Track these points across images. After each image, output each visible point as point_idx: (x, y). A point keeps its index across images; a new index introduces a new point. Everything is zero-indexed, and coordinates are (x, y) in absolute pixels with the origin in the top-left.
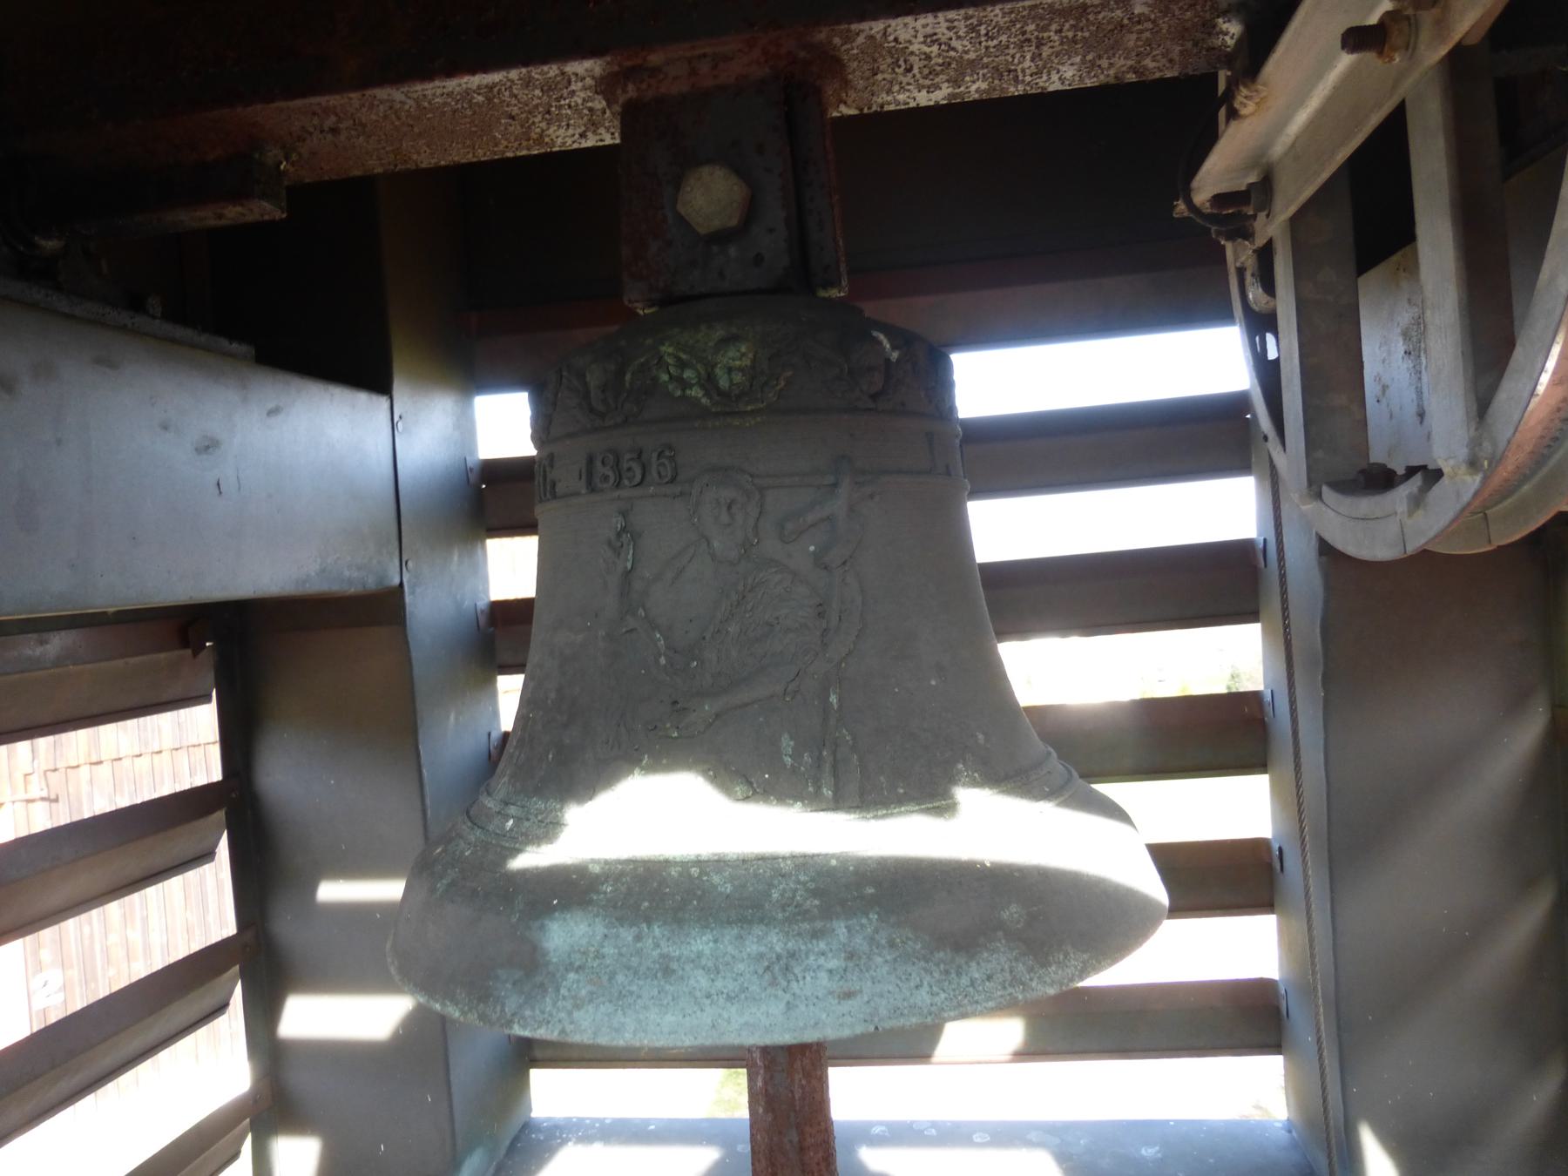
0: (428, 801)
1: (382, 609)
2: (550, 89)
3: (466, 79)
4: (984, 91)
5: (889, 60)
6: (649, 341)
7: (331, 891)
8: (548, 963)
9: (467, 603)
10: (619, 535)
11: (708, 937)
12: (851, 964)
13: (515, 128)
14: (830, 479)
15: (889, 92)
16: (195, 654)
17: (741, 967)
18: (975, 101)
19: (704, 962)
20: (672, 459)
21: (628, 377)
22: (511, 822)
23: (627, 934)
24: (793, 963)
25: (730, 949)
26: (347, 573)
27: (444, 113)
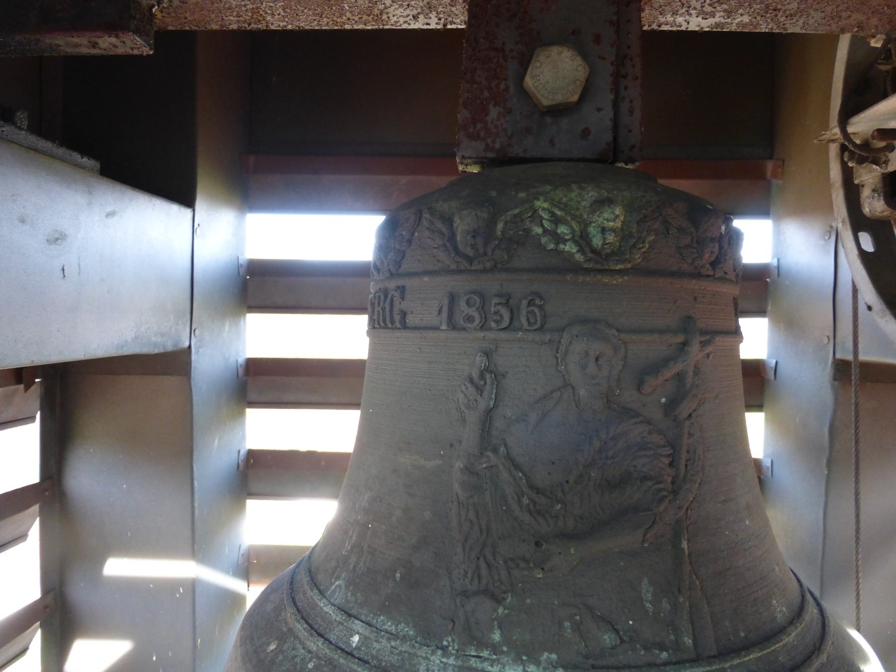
0: (196, 505)
1: (174, 364)
4: (746, 24)
6: (522, 195)
7: (117, 567)
9: (232, 360)
10: (482, 376)
14: (680, 338)
16: (27, 388)
18: (731, 33)
20: (541, 307)
21: (500, 226)
26: (153, 339)
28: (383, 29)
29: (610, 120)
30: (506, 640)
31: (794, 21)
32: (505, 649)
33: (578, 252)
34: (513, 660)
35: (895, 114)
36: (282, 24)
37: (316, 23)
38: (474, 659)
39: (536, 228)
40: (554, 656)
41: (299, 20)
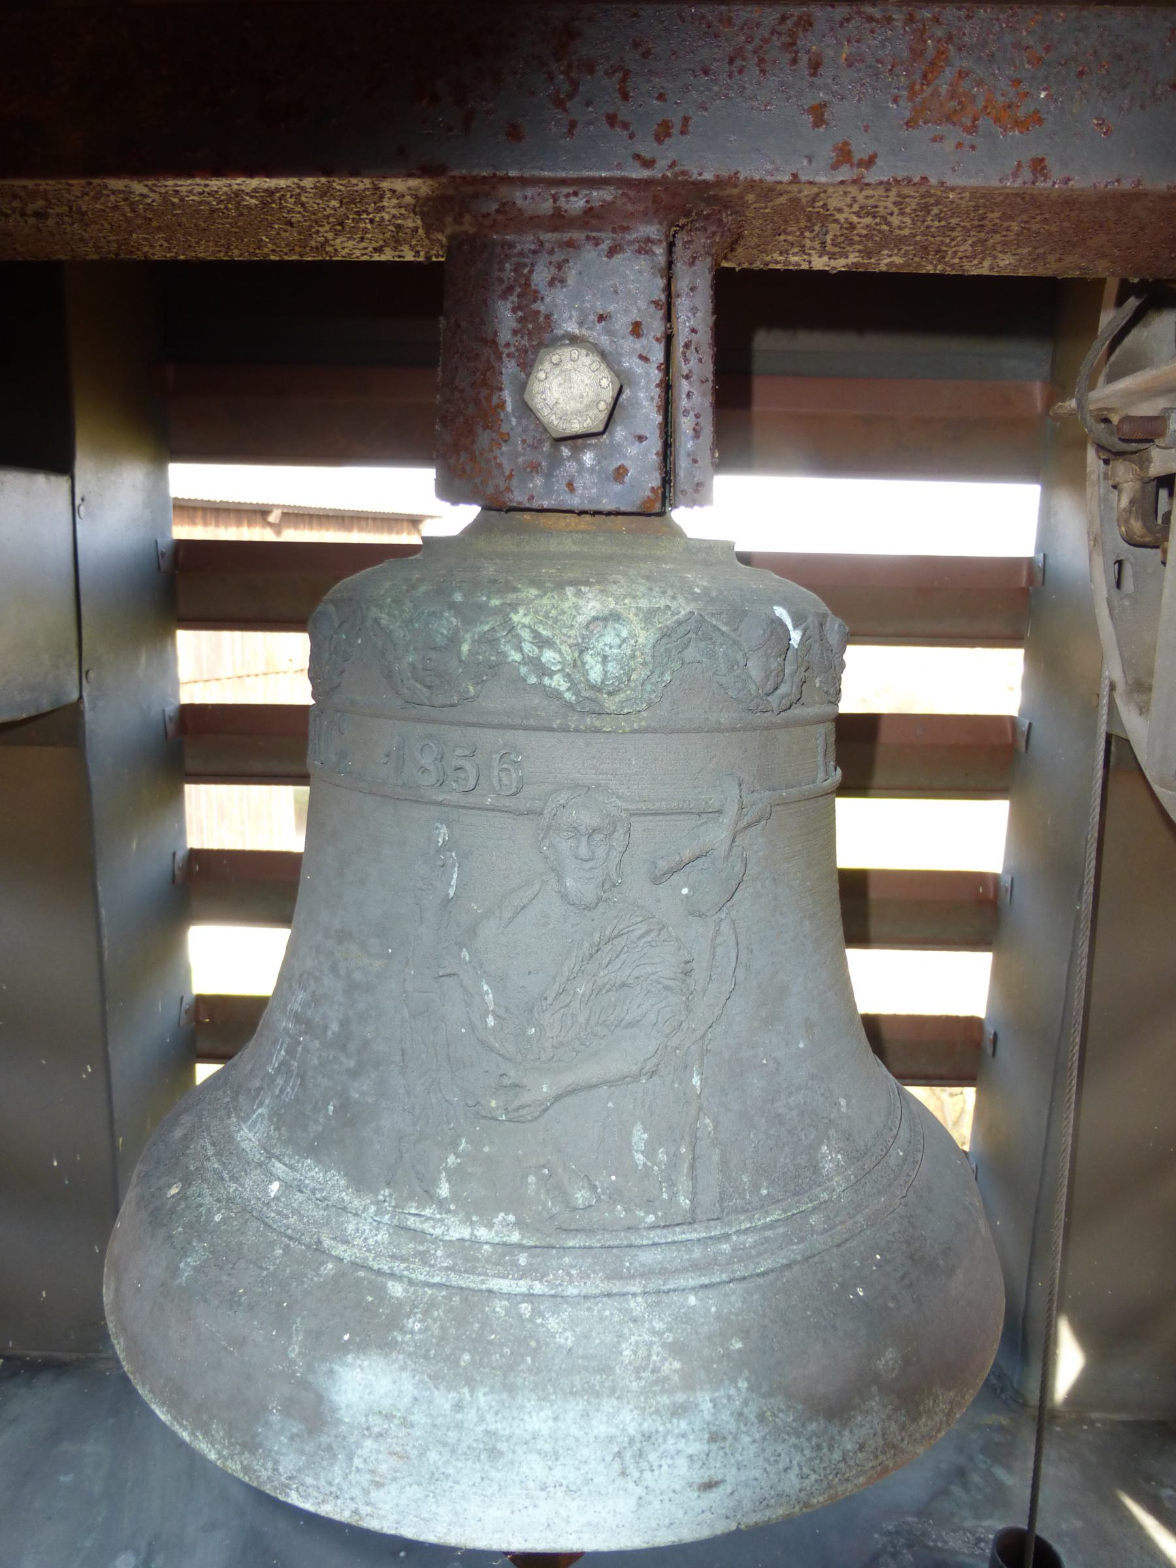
0: (105, 943)
1: (59, 727)
2: (353, 201)
3: (239, 181)
5: (803, 224)
6: (495, 602)
8: (338, 1422)
11: (547, 1413)
12: (714, 1447)
17: (585, 1452)
18: (881, 273)
19: (540, 1444)
22: (275, 1187)
23: (444, 1400)
24: (648, 1447)
25: (574, 1430)
27: (198, 211)
28: (331, 262)
29: (657, 454)
30: (455, 1196)
31: (975, 262)
32: (452, 1207)
33: (568, 689)
34: (461, 1222)
36: (168, 255)
39: (513, 652)
40: (511, 1218)
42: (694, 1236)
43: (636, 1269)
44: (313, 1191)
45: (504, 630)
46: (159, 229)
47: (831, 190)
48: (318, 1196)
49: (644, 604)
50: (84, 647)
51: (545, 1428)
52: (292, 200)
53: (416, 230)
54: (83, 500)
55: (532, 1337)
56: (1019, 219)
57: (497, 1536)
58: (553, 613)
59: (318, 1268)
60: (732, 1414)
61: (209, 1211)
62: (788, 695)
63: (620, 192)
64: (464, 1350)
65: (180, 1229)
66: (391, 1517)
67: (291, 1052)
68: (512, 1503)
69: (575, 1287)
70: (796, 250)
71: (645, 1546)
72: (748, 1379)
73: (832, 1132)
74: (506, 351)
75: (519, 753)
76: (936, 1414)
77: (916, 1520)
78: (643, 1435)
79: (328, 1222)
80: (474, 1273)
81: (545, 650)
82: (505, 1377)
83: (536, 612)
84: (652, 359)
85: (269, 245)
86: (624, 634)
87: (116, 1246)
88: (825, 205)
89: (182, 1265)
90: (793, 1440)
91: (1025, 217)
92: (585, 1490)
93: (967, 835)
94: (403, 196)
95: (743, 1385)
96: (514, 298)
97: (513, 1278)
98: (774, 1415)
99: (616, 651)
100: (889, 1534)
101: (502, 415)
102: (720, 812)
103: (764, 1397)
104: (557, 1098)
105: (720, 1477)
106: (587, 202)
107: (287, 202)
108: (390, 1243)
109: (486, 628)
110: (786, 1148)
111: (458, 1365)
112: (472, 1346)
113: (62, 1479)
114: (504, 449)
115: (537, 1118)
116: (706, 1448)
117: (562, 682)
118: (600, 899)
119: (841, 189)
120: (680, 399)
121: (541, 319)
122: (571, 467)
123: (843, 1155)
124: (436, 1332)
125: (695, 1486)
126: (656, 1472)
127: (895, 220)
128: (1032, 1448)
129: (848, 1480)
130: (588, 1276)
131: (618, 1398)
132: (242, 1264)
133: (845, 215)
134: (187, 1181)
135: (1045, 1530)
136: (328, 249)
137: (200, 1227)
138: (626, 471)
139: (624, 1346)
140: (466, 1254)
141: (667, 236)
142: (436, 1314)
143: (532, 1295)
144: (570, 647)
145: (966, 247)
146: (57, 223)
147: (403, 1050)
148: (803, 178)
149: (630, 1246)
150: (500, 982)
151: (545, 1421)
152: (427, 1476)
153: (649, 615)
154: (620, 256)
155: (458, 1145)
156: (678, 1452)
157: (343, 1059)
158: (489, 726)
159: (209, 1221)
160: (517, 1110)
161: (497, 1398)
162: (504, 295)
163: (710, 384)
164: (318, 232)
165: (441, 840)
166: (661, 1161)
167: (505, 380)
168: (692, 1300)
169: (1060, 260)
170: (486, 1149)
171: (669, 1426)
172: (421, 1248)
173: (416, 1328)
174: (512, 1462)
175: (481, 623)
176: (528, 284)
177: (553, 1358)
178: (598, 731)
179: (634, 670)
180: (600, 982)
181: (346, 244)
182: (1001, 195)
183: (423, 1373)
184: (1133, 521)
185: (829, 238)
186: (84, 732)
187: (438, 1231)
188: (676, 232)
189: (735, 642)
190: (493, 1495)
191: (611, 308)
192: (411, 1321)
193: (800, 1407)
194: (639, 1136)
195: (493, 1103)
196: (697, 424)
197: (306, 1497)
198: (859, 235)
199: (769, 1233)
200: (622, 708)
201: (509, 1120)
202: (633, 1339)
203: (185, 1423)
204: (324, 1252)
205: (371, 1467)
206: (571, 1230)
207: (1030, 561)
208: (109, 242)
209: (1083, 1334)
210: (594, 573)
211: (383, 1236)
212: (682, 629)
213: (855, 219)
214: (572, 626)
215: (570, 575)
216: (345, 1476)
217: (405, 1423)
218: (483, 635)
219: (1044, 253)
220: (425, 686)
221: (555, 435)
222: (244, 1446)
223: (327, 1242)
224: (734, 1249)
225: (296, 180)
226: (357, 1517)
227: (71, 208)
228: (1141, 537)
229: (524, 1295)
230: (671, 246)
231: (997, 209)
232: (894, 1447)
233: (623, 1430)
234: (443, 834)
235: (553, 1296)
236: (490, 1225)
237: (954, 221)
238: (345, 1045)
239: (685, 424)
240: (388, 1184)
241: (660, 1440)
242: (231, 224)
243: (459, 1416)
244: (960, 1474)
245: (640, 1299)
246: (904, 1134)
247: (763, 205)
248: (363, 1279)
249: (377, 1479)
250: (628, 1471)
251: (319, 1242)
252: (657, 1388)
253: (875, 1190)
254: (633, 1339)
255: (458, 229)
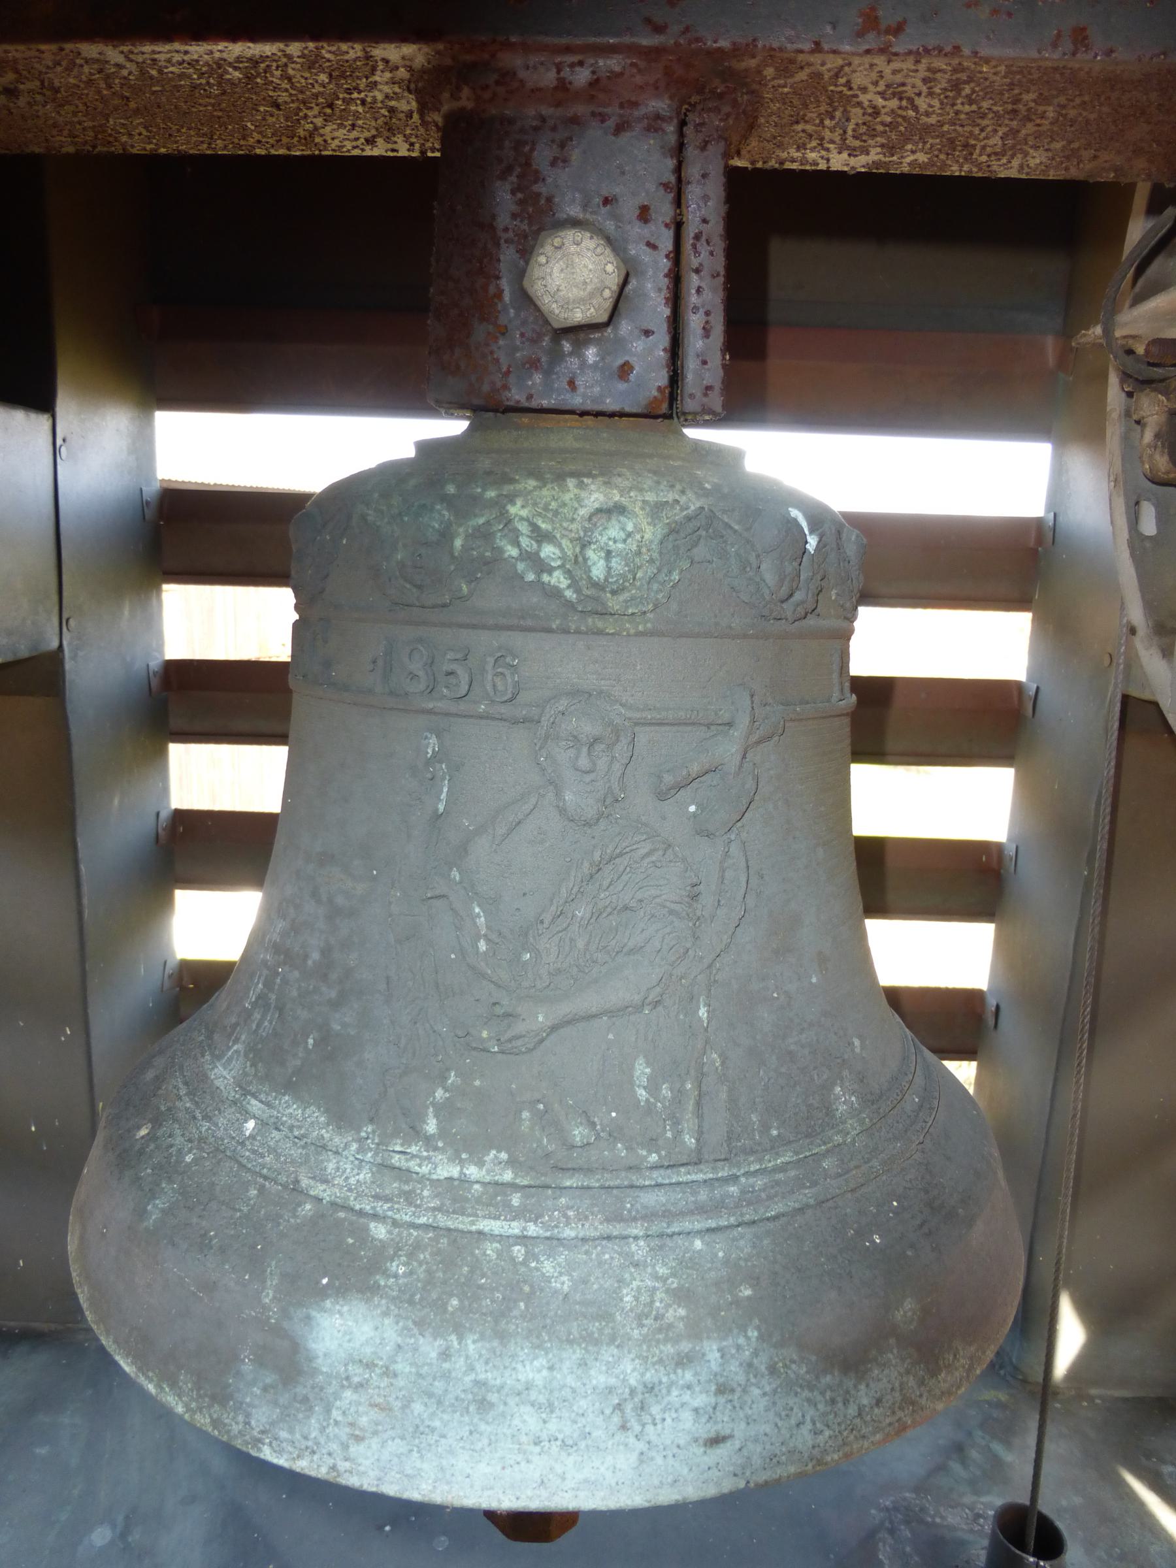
0: (85, 901)
2: (343, 76)
3: (221, 46)
5: (823, 109)
6: (491, 494)
8: (315, 1372)
9: (139, 665)
11: (541, 1362)
12: (722, 1400)
13: (278, 120)
15: (801, 147)
18: (902, 175)
19: (533, 1395)
22: (251, 1124)
23: (430, 1348)
24: (650, 1399)
25: (570, 1381)
27: (178, 88)
28: (320, 156)
29: (665, 350)
30: (443, 1132)
31: (1004, 161)
32: (440, 1144)
33: (569, 587)
34: (449, 1159)
35: (1175, 316)
36: (149, 147)
37: (205, 146)
38: (398, 1156)
39: (509, 547)
40: (504, 1156)
41: (176, 142)
42: (700, 1177)
43: (637, 1211)
44: (291, 1128)
45: (499, 523)
46: (137, 111)
47: (856, 61)
48: (296, 1133)
49: (651, 497)
50: (65, 594)
51: (539, 1379)
52: (278, 73)
53: (409, 115)
54: (64, 440)
55: (525, 1282)
56: (1056, 101)
57: (487, 1493)
58: (554, 505)
59: (295, 1210)
60: (741, 1364)
61: (180, 1151)
62: (803, 602)
63: (629, 61)
64: (451, 1295)
65: (149, 1171)
66: (371, 1474)
67: (268, 985)
68: (503, 1458)
69: (572, 1229)
70: (814, 143)
71: (647, 1505)
72: (758, 1328)
73: (846, 1073)
74: (504, 236)
75: (514, 657)
76: (956, 1369)
77: (914, 1496)
78: (645, 1386)
79: (307, 1161)
80: (463, 1214)
81: (544, 545)
82: (496, 1322)
83: (535, 504)
84: (661, 246)
85: (255, 134)
86: (630, 527)
87: (82, 1192)
88: (849, 82)
89: (149, 1207)
90: (806, 1393)
91: (1062, 100)
92: (582, 1444)
93: (966, 803)
94: (397, 68)
95: (753, 1334)
96: (513, 179)
97: (505, 1220)
98: (785, 1366)
99: (620, 546)
100: (887, 1509)
101: (500, 307)
102: (730, 724)
103: (775, 1346)
104: (554, 1028)
105: (727, 1432)
106: (593, 72)
107: (273, 76)
108: (373, 1182)
109: (481, 521)
110: (798, 1088)
111: (445, 1311)
112: (459, 1291)
113: (38, 1451)
114: (501, 342)
115: (530, 1051)
116: (713, 1400)
117: (562, 579)
118: (601, 815)
119: (867, 59)
120: (689, 294)
121: (543, 202)
122: (573, 363)
123: (857, 1098)
124: (422, 1276)
125: (701, 1442)
126: (659, 1426)
127: (922, 103)
128: (1033, 1425)
129: (864, 1437)
130: (586, 1218)
131: (618, 1347)
132: (214, 1205)
133: (869, 96)
134: (157, 1122)
135: (1046, 1506)
136: (318, 140)
137: (170, 1169)
138: (632, 368)
139: (625, 1291)
140: (454, 1193)
141: (678, 113)
142: (422, 1256)
143: (525, 1237)
144: (571, 541)
145: (996, 140)
146: (29, 103)
147: (388, 978)
148: (826, 47)
149: (632, 1186)
150: (492, 904)
151: (539, 1371)
152: (411, 1430)
153: (656, 510)
154: (628, 134)
155: (446, 1078)
156: (683, 1405)
157: (324, 989)
158: (484, 627)
159: (179, 1162)
160: (510, 1041)
161: (488, 1345)
162: (503, 176)
163: (721, 279)
164: (306, 116)
165: (430, 751)
166: (665, 1098)
167: (503, 267)
168: (698, 1244)
169: (1095, 157)
170: (477, 1083)
171: (673, 1376)
172: (406, 1188)
173: (400, 1272)
174: (503, 1415)
175: (475, 516)
176: (528, 164)
177: (548, 1304)
178: (600, 633)
179: (639, 568)
180: (601, 905)
181: (336, 134)
182: (1039, 68)
183: (407, 1318)
184: (1157, 457)
185: (851, 126)
186: (64, 682)
187: (425, 1169)
188: (687, 110)
189: (748, 542)
190: (482, 1449)
191: (617, 190)
192: (394, 1264)
193: (814, 1358)
194: (642, 1070)
195: (485, 1034)
196: (707, 322)
197: (280, 1452)
198: (883, 124)
199: (780, 1176)
200: (627, 608)
201: (502, 1052)
202: (635, 1284)
203: (150, 1374)
204: (302, 1192)
205: (350, 1419)
206: (568, 1169)
207: (1039, 522)
208: (84, 129)
209: (1084, 1309)
210: (601, 468)
211: (365, 1175)
212: (692, 525)
213: (880, 102)
214: (573, 520)
215: (572, 467)
216: (323, 1429)
217: (388, 1372)
218: (477, 529)
219: (1079, 148)
220: (415, 586)
221: (556, 325)
222: (214, 1398)
223: (305, 1182)
224: (743, 1192)
225: (281, 45)
226: (335, 1474)
227: (42, 82)
228: (1168, 473)
229: (518, 1237)
230: (683, 124)
231: (1033, 88)
232: (913, 1403)
233: (624, 1380)
234: (432, 745)
235: (547, 1238)
236: (480, 1164)
237: (985, 104)
238: (326, 975)
239: (694, 322)
240: (371, 1120)
241: (664, 1391)
242: (213, 105)
243: (446, 1365)
244: (959, 1449)
245: (642, 1243)
246: (919, 1080)
247: (782, 82)
248: (345, 1219)
249: (357, 1432)
250: (629, 1425)
251: (297, 1182)
252: (661, 1337)
253: (890, 1135)
254: (635, 1284)
255: (456, 105)
